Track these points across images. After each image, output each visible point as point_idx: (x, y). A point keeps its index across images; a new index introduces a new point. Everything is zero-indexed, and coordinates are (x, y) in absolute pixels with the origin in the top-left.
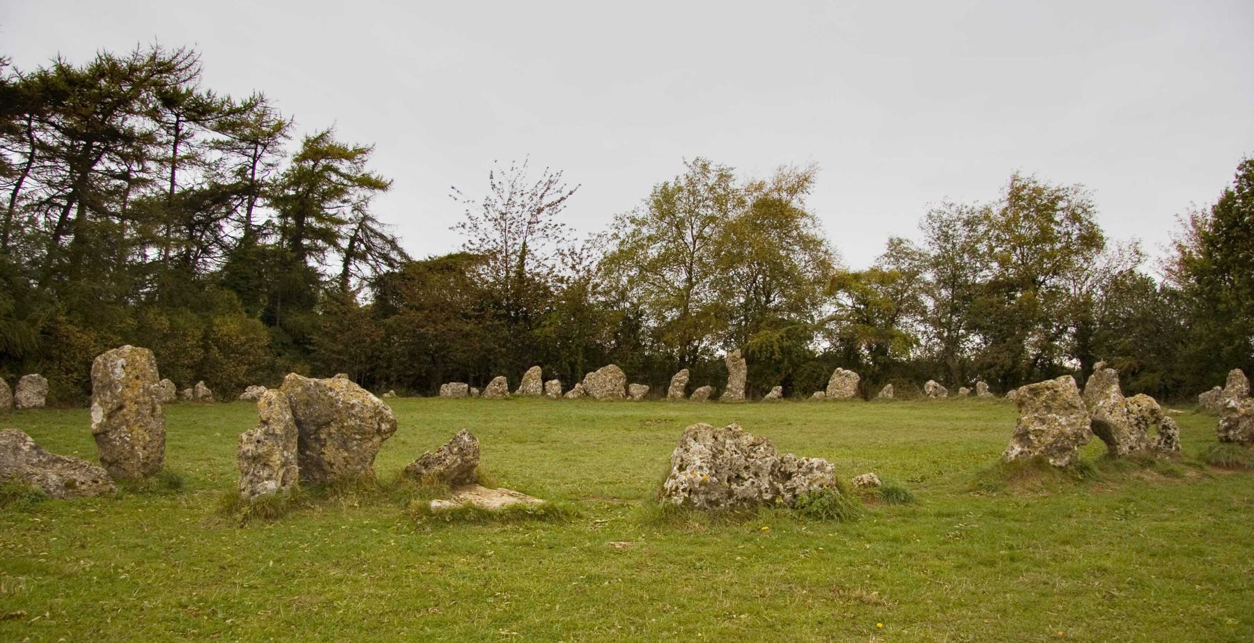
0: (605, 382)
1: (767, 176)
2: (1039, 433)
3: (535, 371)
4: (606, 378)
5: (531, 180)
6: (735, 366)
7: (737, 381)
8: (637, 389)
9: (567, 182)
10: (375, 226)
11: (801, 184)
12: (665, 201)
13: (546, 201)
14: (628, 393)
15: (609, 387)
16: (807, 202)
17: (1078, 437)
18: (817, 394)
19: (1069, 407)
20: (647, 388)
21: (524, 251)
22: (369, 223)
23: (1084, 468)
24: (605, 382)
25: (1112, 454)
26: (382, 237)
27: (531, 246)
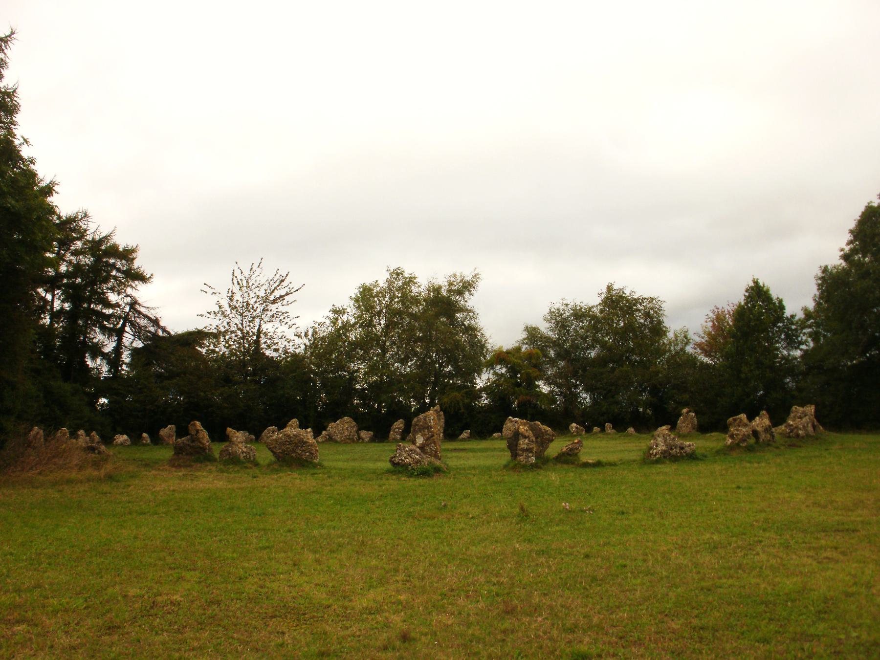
0: (343, 430)
1: (442, 281)
2: (737, 435)
4: (343, 426)
5: (264, 277)
8: (365, 435)
9: (294, 281)
10: (142, 310)
11: (467, 286)
12: (365, 297)
13: (277, 294)
15: (346, 433)
16: (472, 301)
17: (749, 435)
19: (746, 425)
21: (259, 331)
22: (137, 307)
23: (751, 446)
25: (757, 442)
26: (146, 317)
27: (264, 327)
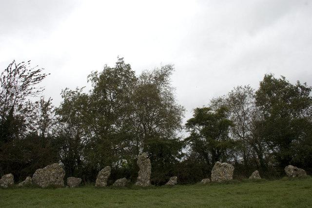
0: (49, 175)
3: (204, 183)
6: (143, 163)
7: (145, 175)
14: (66, 184)
18: (204, 181)
20: (80, 180)
24: (49, 175)
